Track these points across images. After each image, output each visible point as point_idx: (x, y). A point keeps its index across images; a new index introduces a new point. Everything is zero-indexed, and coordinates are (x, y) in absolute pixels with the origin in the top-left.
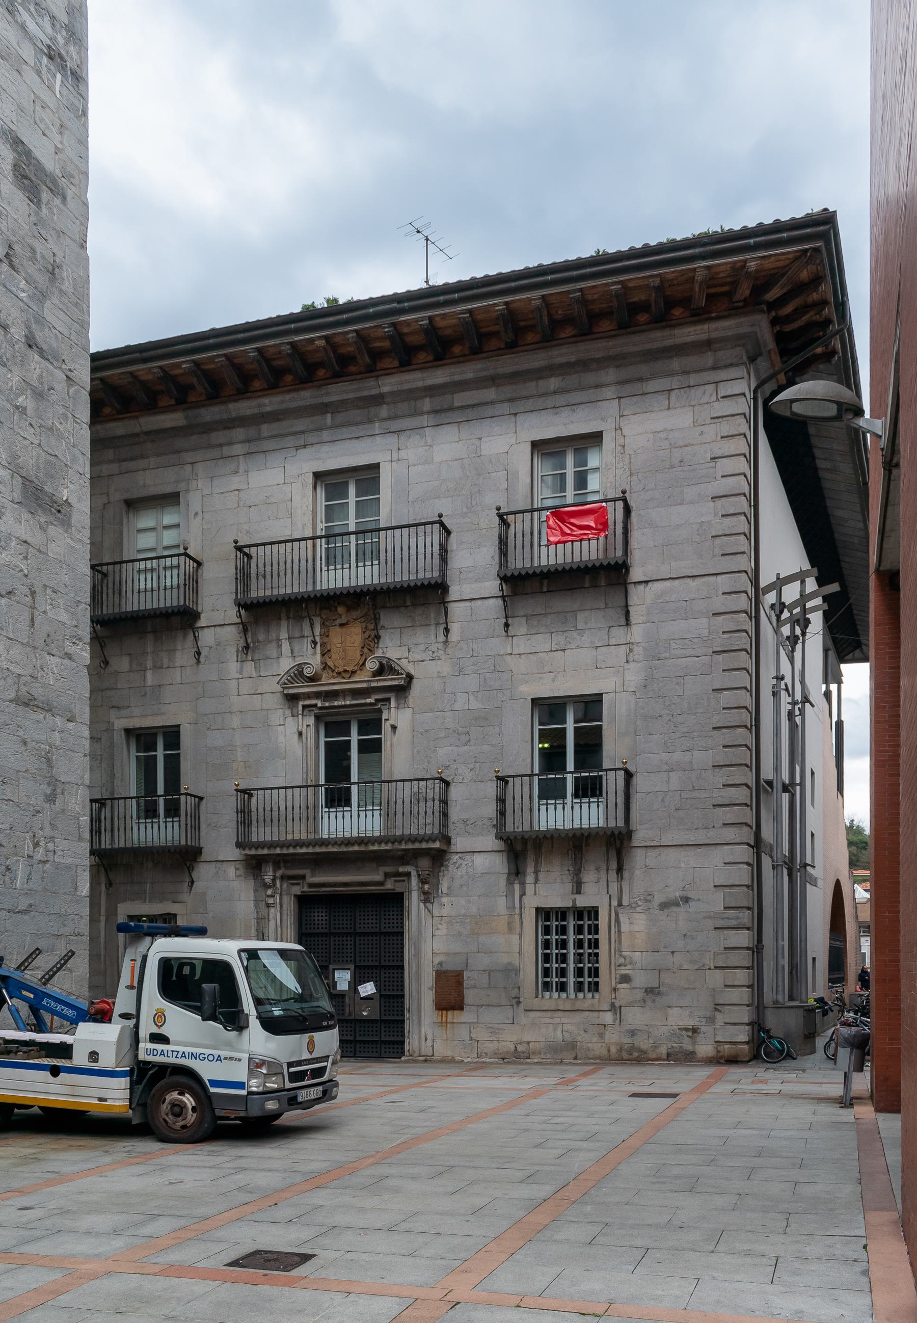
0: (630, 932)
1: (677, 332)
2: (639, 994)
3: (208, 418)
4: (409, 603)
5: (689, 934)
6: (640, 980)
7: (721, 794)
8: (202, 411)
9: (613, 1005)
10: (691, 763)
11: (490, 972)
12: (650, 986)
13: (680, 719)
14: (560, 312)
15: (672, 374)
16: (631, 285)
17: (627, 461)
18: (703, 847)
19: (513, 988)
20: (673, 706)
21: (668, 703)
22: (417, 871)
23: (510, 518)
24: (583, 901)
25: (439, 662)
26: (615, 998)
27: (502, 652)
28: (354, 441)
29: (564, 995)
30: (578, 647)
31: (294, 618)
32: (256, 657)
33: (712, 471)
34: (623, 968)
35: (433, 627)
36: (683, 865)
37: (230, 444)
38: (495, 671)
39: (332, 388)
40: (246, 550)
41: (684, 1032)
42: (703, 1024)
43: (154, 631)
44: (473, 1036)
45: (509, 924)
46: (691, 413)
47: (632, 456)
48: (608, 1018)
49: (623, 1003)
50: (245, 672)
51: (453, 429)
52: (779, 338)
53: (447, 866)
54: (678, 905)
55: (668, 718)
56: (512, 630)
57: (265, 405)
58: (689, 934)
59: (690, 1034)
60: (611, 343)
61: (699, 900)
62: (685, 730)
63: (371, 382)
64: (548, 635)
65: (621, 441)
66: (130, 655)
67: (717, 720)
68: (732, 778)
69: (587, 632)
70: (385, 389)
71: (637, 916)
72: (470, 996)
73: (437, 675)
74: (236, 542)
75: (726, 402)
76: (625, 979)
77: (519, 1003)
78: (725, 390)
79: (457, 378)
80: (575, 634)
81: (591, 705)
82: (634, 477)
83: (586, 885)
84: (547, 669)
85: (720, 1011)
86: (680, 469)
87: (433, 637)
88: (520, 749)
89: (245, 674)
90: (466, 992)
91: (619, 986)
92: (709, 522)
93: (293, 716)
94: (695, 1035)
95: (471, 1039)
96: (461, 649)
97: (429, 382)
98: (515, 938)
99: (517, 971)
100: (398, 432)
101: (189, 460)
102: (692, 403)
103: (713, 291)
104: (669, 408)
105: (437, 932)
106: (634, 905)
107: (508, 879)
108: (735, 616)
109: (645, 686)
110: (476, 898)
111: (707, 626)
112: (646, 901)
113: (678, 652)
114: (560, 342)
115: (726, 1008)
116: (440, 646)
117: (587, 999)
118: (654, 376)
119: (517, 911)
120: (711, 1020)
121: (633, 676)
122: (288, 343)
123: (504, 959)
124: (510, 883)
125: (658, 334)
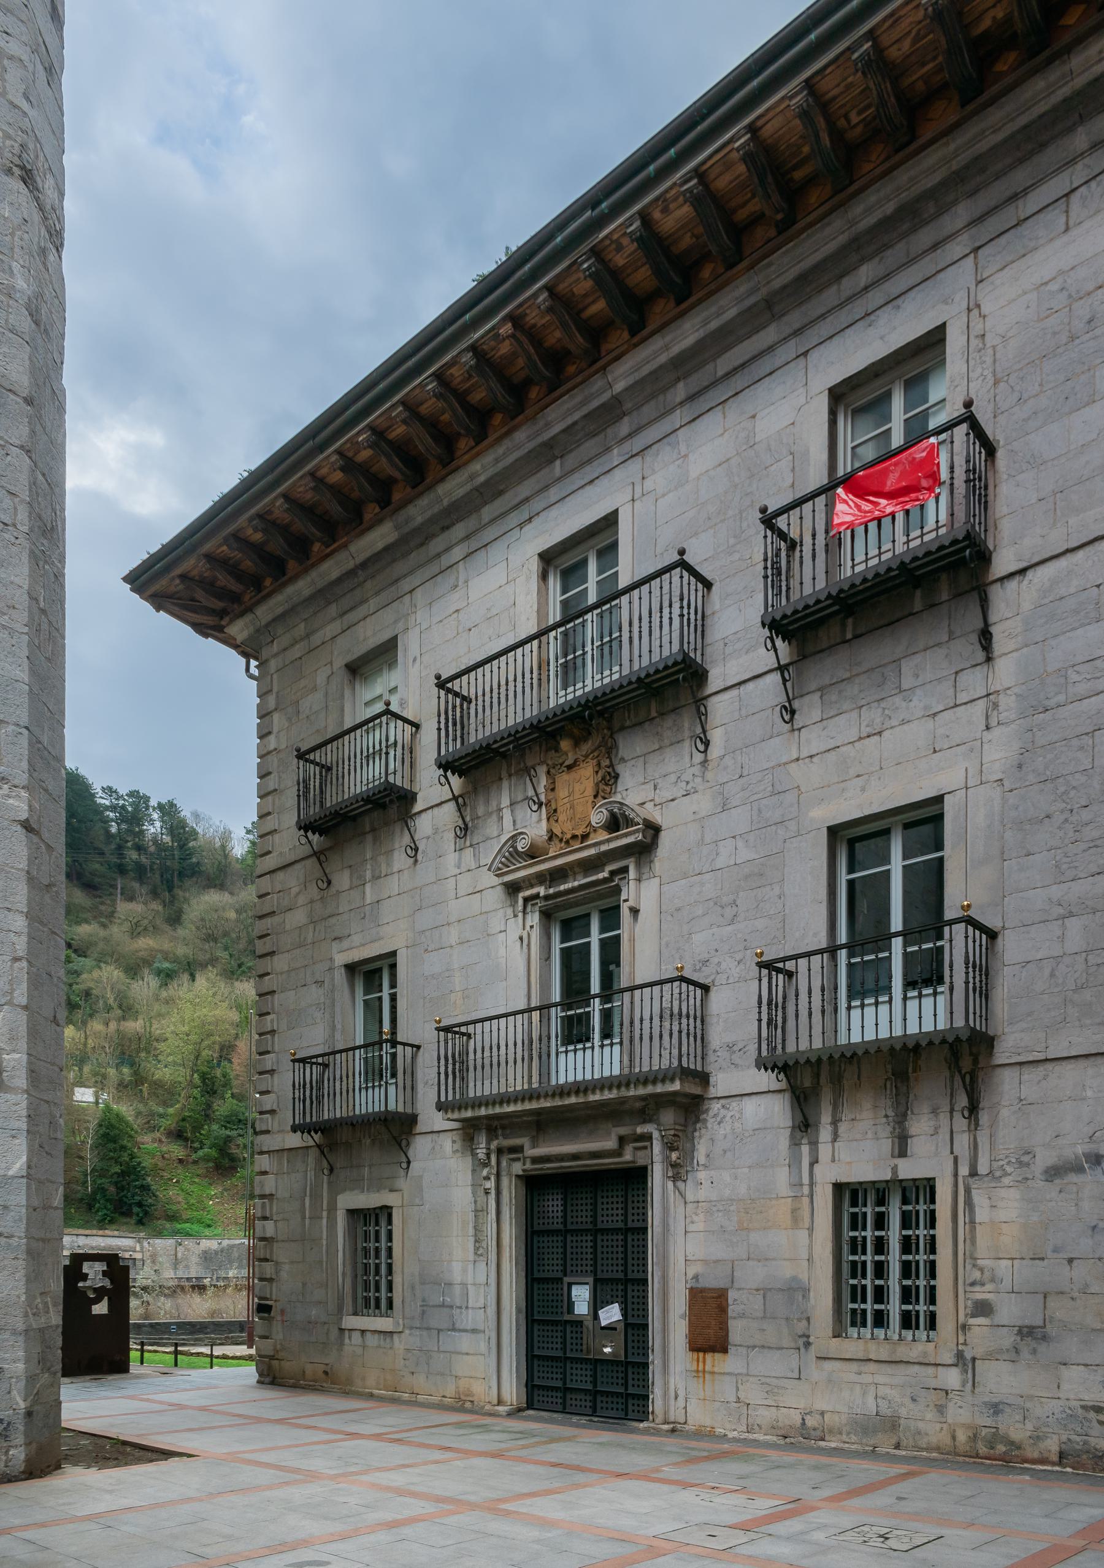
2: (1008, 1339)
4: (654, 714)
6: (1010, 1311)
9: (960, 1355)
11: (765, 1292)
12: (1027, 1322)
14: (855, 119)
19: (799, 1320)
20: (1073, 793)
21: (1062, 789)
23: (781, 522)
25: (695, 796)
29: (880, 1333)
30: (903, 722)
34: (977, 1288)
39: (553, 413)
40: (449, 685)
48: (952, 1378)
49: (979, 1352)
50: (463, 864)
53: (705, 1120)
54: (1080, 1170)
55: (1063, 817)
56: (799, 720)
64: (855, 714)
69: (918, 692)
71: (1003, 1193)
72: (737, 1330)
74: (438, 677)
76: (983, 1309)
80: (897, 700)
83: (915, 1140)
84: (852, 772)
87: (687, 758)
91: (972, 1321)
95: (738, 1401)
99: (806, 1292)
105: (690, 1228)
106: (998, 1174)
107: (792, 1136)
110: (746, 1170)
116: (696, 770)
119: (806, 1190)
123: (787, 1271)
124: (795, 1144)
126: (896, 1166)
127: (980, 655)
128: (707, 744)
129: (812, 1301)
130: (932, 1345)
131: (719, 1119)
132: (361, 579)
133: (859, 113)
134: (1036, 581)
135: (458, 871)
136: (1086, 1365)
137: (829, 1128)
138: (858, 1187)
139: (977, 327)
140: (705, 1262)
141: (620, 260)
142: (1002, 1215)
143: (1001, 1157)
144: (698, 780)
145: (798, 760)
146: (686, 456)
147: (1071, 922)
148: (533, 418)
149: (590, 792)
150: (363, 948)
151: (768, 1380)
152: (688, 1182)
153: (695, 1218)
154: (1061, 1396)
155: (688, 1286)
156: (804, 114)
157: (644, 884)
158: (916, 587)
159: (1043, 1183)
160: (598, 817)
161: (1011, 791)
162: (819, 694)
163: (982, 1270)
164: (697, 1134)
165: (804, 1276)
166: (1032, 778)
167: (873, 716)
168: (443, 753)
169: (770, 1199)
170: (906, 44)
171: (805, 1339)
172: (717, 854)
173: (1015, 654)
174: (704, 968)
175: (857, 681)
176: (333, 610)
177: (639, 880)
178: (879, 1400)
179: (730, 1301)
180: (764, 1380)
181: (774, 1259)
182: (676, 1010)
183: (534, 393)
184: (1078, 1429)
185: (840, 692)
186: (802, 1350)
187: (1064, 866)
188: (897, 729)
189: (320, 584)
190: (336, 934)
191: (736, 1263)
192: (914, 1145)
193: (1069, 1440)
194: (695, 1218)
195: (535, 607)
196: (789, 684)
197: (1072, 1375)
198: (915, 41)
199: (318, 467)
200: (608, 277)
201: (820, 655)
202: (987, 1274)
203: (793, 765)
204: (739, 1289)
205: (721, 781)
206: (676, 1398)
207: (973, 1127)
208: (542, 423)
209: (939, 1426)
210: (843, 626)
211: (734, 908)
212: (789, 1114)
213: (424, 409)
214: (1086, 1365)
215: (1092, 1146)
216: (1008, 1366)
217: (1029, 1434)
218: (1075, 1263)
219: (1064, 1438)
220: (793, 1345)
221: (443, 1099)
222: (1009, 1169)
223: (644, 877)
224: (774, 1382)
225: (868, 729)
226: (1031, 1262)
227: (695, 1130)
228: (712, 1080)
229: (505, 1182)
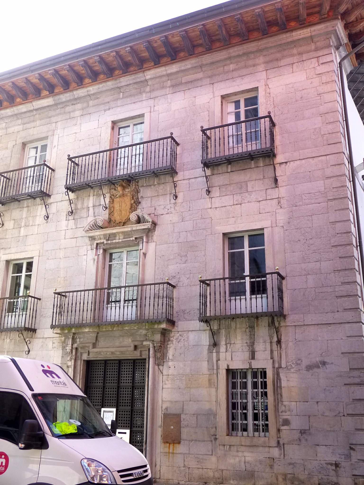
0: (288, 387)
1: (294, 34)
2: (297, 435)
3: (64, 100)
4: (156, 183)
5: (327, 388)
6: (296, 423)
7: (340, 289)
8: (61, 96)
9: (278, 442)
10: (320, 269)
11: (197, 415)
12: (303, 428)
13: (311, 242)
14: (232, 29)
15: (293, 55)
16: (266, 9)
17: (272, 101)
18: (332, 325)
19: (212, 428)
20: (306, 234)
21: (303, 232)
22: (153, 344)
23: (208, 132)
24: (257, 365)
25: (171, 215)
26: (280, 438)
27: (206, 207)
28: (133, 104)
29: (245, 433)
30: (249, 202)
31: (97, 195)
32: (76, 218)
33: (319, 100)
34: (284, 414)
35: (168, 196)
36: (320, 338)
37: (74, 111)
38: (201, 218)
39: (122, 79)
40: (73, 160)
41: (329, 466)
42: (343, 460)
43: (28, 207)
44: (186, 463)
45: (209, 380)
46: (305, 74)
47: (275, 98)
48: (276, 452)
49: (285, 441)
50: (69, 226)
51: (182, 93)
52: (351, 37)
53: (172, 341)
54: (319, 367)
55: (304, 241)
56: (212, 194)
57: (90, 91)
58: (327, 388)
59: (334, 468)
60: (260, 43)
61: (332, 363)
62: (315, 248)
63: (141, 75)
64: (232, 196)
65: (268, 91)
66: (14, 220)
67: (333, 241)
68: (347, 278)
69: (253, 193)
70: (148, 77)
71: (292, 375)
72: (185, 433)
73: (169, 222)
74: (69, 156)
75: (324, 66)
76: (286, 422)
77: (216, 439)
78: (322, 60)
79: (183, 68)
80: (247, 194)
81: (257, 238)
82: (276, 108)
83: (258, 353)
84: (231, 216)
85: (354, 450)
86: (301, 102)
87: (168, 201)
88: (215, 263)
89: (69, 227)
90: (182, 430)
91: (282, 428)
92: (320, 128)
93: (91, 249)
94: (338, 469)
95: (184, 466)
96: (183, 207)
97: (169, 72)
98: (213, 390)
99: (215, 415)
100: (154, 98)
101: (55, 121)
102: (306, 69)
103: (311, 11)
104: (293, 72)
105: (164, 386)
106: (289, 367)
107: (209, 349)
108: (339, 178)
109: (289, 223)
110: (190, 362)
111: (323, 185)
112: (297, 364)
113: (307, 201)
114: (234, 45)
115: (359, 447)
116: (172, 206)
117: (261, 438)
118: (283, 57)
119: (215, 371)
120: (348, 457)
121: (282, 217)
122: (97, 56)
123: (207, 406)
124: (210, 352)
125: (284, 36)
126: (251, 362)
127: (274, 185)
128: (176, 197)
129: (218, 419)
130: (267, 438)
131: (178, 340)
132: (34, 114)
133: (234, 29)
134: (290, 166)
135: (66, 228)
136: (326, 446)
137: (225, 347)
138: (235, 371)
139: (268, 91)
140: (171, 402)
141: (155, 45)
142: (291, 384)
143: (290, 361)
144: (173, 209)
145: (211, 208)
146: (170, 103)
147: (309, 277)
148: (116, 79)
149: (129, 206)
150: (17, 254)
151: (198, 456)
152: (164, 366)
153: (167, 382)
154: (318, 459)
155: (163, 412)
156: (219, 26)
157: (150, 244)
158: (252, 160)
159: (306, 372)
160: (133, 217)
161: (286, 230)
162: (219, 187)
163: (285, 406)
164: (168, 346)
165: (214, 409)
166: (293, 227)
167: (238, 198)
168: (68, 183)
169: (200, 375)
170: (249, 18)
171: (215, 437)
172: (180, 237)
173: (285, 187)
174: (173, 279)
175: (232, 186)
176: (19, 121)
177: (147, 242)
178: (246, 464)
179: (182, 420)
180: (196, 456)
181: (201, 401)
182: (161, 295)
183: (117, 72)
184: (325, 473)
185: (226, 188)
186: (213, 442)
187: (306, 258)
188: (247, 204)
189: (16, 112)
190: (3, 247)
191: (184, 402)
192: (257, 355)
193: (322, 478)
194: (167, 382)
195: (109, 138)
196: (208, 182)
197: (321, 450)
198: (252, 17)
199: (29, 77)
200: (150, 47)
201: (219, 175)
202: (287, 408)
203: (209, 210)
204: (186, 414)
205: (181, 211)
206: (156, 466)
207: (279, 349)
208: (118, 81)
209: (271, 474)
210: (227, 167)
211: (186, 258)
212: (208, 340)
213: (76, 68)
214: (326, 446)
215: (322, 358)
216: (296, 447)
217: (306, 476)
218: (319, 403)
219: (320, 477)
220: (209, 439)
221: (54, 324)
222: (293, 366)
223: (150, 241)
224: (201, 457)
225: (236, 202)
226: (303, 403)
227: (168, 344)
228: (176, 324)
229: (79, 362)
